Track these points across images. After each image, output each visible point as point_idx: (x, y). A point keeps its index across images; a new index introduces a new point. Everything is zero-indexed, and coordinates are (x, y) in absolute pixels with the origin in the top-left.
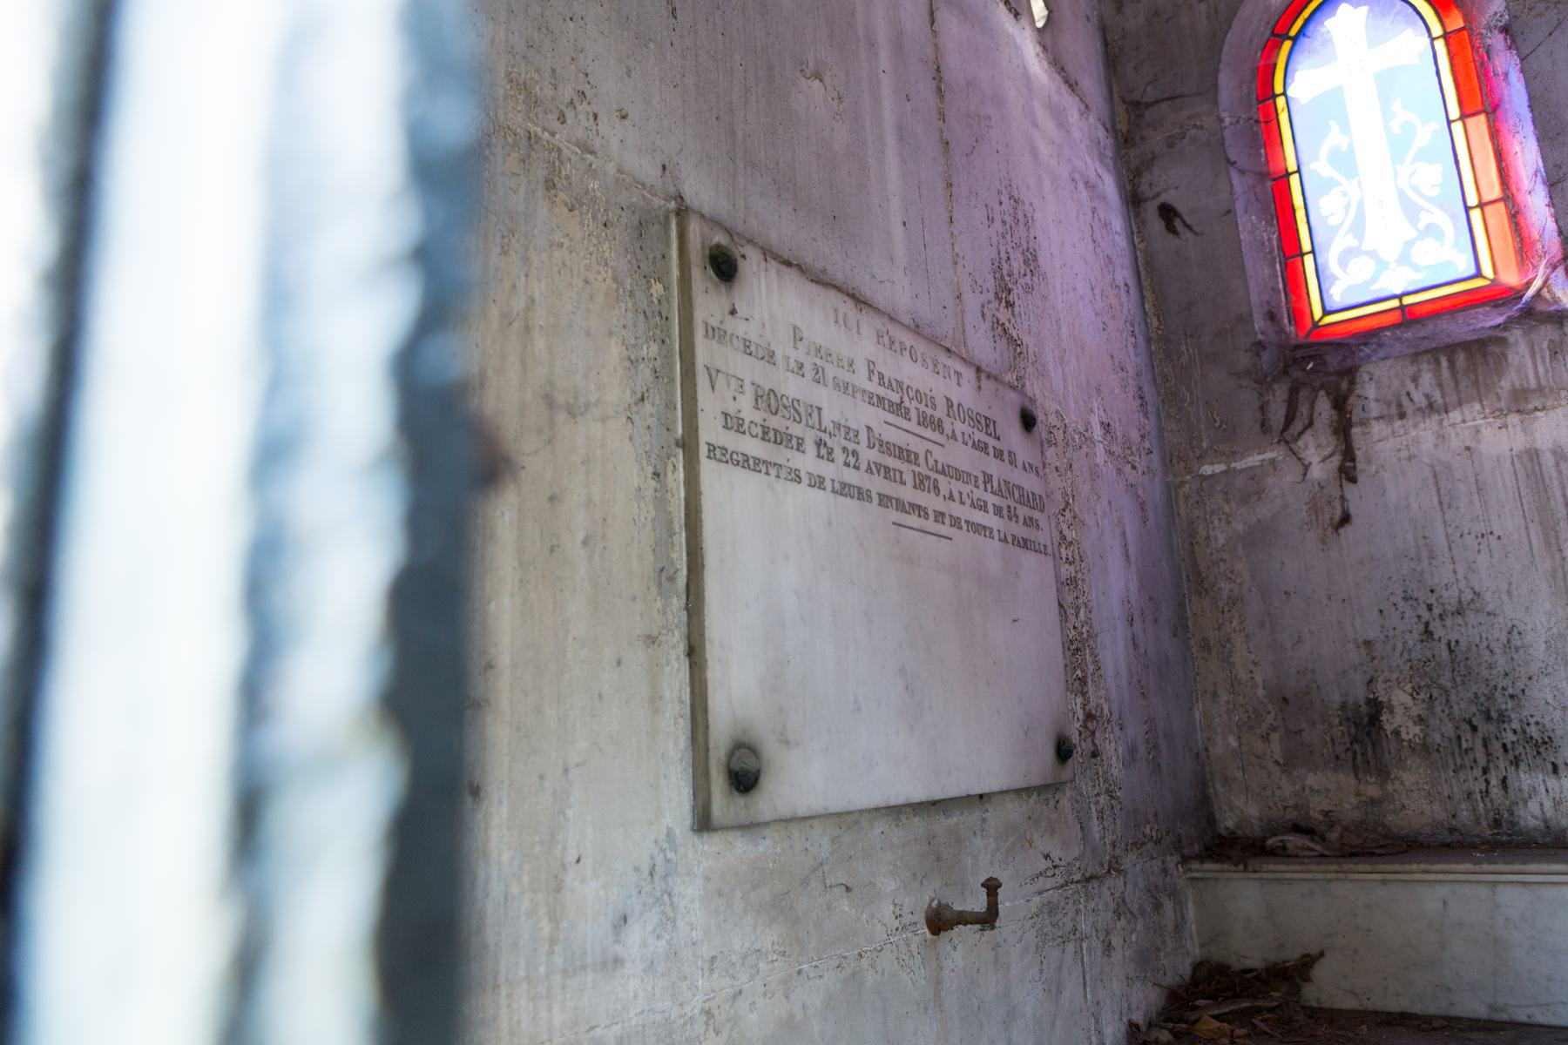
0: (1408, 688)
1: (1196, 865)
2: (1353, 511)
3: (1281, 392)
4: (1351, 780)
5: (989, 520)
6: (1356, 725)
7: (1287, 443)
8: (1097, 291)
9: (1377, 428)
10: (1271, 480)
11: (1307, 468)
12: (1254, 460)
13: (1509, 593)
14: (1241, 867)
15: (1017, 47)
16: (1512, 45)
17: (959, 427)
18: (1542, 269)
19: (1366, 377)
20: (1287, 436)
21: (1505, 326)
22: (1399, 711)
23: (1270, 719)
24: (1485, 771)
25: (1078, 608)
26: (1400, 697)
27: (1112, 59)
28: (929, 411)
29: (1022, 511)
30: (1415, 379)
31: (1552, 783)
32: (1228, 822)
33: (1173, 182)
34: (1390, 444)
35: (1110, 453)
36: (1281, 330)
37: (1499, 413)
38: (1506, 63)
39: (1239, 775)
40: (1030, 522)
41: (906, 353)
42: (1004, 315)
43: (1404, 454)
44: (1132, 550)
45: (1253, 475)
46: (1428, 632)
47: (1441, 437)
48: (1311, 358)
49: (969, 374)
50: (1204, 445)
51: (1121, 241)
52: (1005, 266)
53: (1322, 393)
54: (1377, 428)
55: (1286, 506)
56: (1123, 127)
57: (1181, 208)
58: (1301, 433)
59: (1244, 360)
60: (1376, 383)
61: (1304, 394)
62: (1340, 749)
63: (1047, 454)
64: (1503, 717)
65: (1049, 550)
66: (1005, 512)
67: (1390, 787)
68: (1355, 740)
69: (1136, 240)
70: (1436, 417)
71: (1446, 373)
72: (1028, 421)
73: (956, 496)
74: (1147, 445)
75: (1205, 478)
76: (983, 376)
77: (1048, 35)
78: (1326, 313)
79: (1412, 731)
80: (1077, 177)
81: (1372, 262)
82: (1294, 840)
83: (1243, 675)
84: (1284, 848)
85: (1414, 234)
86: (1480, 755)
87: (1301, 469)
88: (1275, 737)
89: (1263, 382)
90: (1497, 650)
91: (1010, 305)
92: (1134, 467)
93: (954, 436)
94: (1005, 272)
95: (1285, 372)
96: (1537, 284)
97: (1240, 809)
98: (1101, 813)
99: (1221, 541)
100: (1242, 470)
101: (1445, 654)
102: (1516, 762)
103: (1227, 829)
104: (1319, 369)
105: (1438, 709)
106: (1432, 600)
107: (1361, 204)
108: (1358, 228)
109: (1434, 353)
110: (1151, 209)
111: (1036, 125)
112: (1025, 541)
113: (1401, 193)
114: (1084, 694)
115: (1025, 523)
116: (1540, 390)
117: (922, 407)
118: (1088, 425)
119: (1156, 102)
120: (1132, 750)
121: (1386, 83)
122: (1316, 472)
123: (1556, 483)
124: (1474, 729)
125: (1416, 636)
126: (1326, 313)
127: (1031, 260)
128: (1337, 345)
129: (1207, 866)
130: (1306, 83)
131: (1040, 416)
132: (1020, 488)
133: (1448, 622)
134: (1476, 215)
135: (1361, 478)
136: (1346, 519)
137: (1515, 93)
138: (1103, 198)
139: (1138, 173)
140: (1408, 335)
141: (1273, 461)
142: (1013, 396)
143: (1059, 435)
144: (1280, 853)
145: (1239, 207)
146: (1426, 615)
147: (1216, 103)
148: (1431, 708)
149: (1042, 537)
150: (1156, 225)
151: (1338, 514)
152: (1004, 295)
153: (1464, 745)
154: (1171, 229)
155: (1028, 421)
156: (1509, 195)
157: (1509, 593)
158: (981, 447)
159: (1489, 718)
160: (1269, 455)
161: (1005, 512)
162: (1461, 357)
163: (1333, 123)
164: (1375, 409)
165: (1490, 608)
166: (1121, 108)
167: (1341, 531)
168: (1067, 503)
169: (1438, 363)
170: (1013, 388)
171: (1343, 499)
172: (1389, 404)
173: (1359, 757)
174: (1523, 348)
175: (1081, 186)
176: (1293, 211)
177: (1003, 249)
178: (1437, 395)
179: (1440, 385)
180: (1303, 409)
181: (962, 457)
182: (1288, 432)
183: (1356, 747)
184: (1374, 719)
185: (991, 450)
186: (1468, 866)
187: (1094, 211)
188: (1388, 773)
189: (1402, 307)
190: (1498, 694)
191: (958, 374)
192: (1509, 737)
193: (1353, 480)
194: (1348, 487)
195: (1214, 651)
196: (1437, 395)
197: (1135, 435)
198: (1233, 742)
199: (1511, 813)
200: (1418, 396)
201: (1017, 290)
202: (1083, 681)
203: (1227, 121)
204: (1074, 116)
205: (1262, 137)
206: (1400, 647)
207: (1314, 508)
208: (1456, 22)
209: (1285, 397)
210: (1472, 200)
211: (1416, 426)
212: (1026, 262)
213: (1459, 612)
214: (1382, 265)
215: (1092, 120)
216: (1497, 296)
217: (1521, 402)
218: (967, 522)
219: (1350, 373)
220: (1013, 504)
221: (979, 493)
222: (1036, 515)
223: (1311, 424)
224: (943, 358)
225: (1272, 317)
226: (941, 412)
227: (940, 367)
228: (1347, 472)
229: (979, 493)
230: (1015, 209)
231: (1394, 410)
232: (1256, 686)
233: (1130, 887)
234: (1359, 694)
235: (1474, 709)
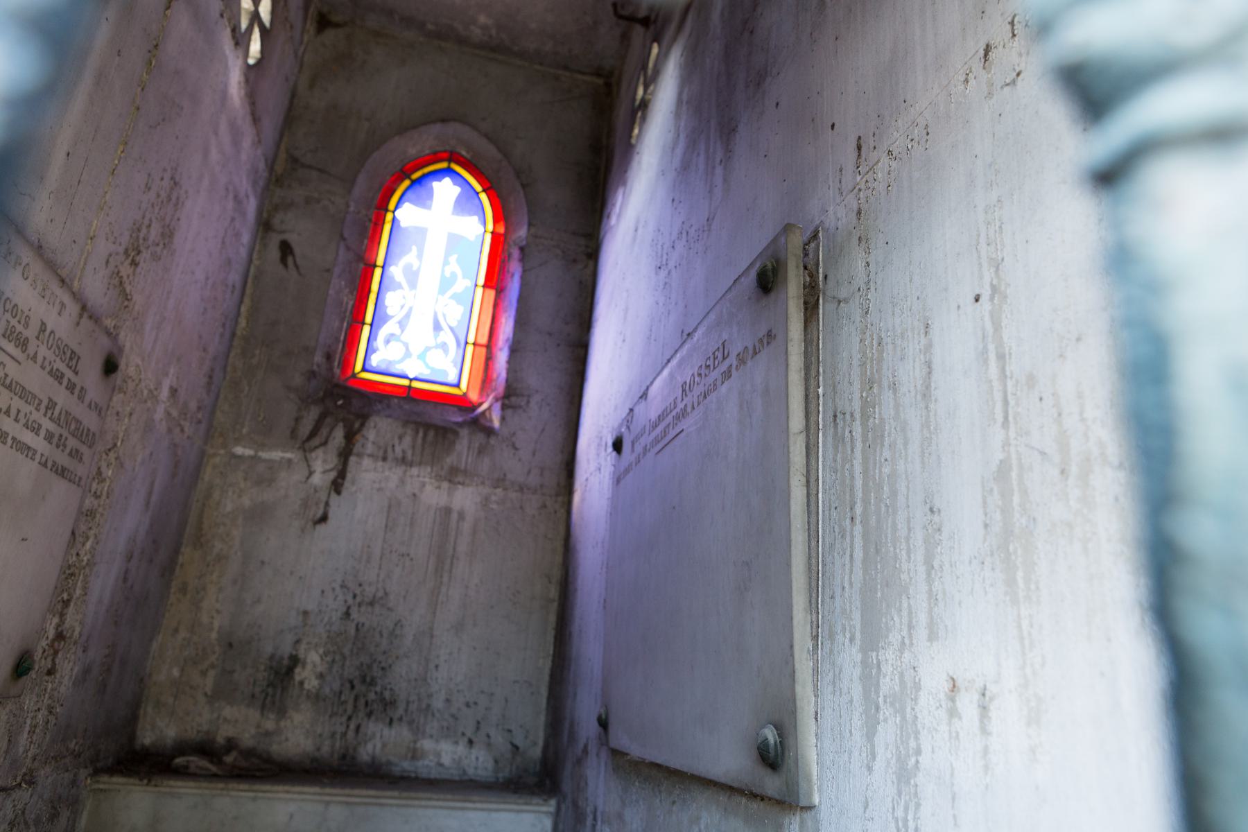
0: (321, 651)
1: (105, 778)
2: (330, 515)
3: (313, 413)
4: (257, 715)
5: (37, 442)
6: (277, 673)
7: (305, 451)
8: (210, 282)
9: (367, 462)
10: (283, 474)
11: (311, 473)
12: (276, 455)
13: (405, 597)
14: (145, 781)
15: (226, 67)
16: (522, 260)
17: (43, 351)
18: (491, 397)
19: (372, 425)
20: (307, 446)
21: (461, 425)
22: (309, 667)
23: (213, 658)
24: (350, 718)
25: (88, 538)
26: (313, 658)
27: (290, 119)
28: (19, 328)
29: (72, 443)
30: (400, 438)
31: (386, 732)
32: (146, 738)
33: (299, 229)
34: (371, 476)
35: (168, 414)
36: (331, 369)
37: (439, 478)
38: (515, 267)
39: (171, 700)
40: (75, 454)
41: (20, 269)
42: (126, 270)
43: (376, 486)
44: (154, 498)
45: (271, 465)
46: (347, 614)
47: (402, 482)
48: (344, 397)
49: (73, 308)
50: (244, 431)
51: (243, 252)
52: (144, 231)
53: (341, 424)
54: (367, 462)
55: (286, 496)
56: (279, 168)
57: (297, 250)
58: (316, 447)
59: (298, 380)
60: (380, 429)
61: (329, 420)
62: (258, 690)
63: (115, 399)
64: (373, 682)
65: (83, 483)
66: (55, 440)
67: (282, 724)
68: (271, 684)
69: (255, 256)
70: (403, 468)
71: (419, 441)
72: (110, 367)
73: (13, 412)
74: (200, 416)
75: (234, 456)
76: (85, 315)
77: (253, 73)
78: (364, 369)
79: (312, 683)
80: (231, 188)
81: (404, 349)
82: (196, 762)
83: (205, 619)
84: (187, 767)
85: (433, 343)
86: (350, 707)
87: (307, 473)
88: (212, 673)
89: (306, 401)
90: (385, 635)
91: (134, 264)
92: (182, 431)
93: (34, 358)
94: (142, 235)
95: (322, 400)
96: (485, 406)
97: (159, 729)
98: (34, 727)
99: (229, 508)
100: (265, 461)
101: (353, 632)
102: (369, 715)
103: (143, 745)
104: (348, 406)
105: (334, 670)
106: (358, 592)
107: (411, 309)
108: (402, 324)
109: (418, 425)
110: (275, 240)
111: (216, 134)
112: (64, 469)
113: (436, 314)
114: (62, 615)
115: (70, 454)
116: (465, 472)
117: (14, 322)
118: (159, 385)
119: (310, 167)
120: (86, 671)
121: (454, 241)
122: (317, 479)
123: (453, 533)
124: (353, 687)
125: (339, 614)
126: (364, 369)
127: (168, 234)
128: (362, 395)
129: (115, 779)
130: (407, 214)
131: (122, 366)
132: (78, 422)
133: (363, 609)
134: (470, 349)
135: (344, 493)
136: (324, 519)
137: (514, 287)
138: (244, 214)
139: (276, 208)
140: (407, 407)
141: (290, 461)
142: (105, 341)
143: (131, 385)
144: (182, 773)
145: (337, 270)
146: (350, 601)
147: (350, 192)
148: (330, 669)
149: (80, 470)
150: (274, 253)
151: (320, 513)
152: (133, 254)
153: (343, 698)
154: (283, 260)
155: (110, 367)
156: (490, 346)
157: (405, 597)
158: (58, 376)
159: (363, 681)
160: (289, 455)
161: (55, 440)
162: (431, 433)
163: (414, 248)
164: (370, 448)
165: (391, 605)
166: (282, 155)
167: (318, 527)
168: (115, 445)
169: (417, 432)
170: (109, 334)
171: (327, 504)
172: (379, 448)
173: (269, 698)
174: (465, 442)
175: (231, 196)
176: (369, 292)
177: (148, 216)
178: (409, 453)
179: (413, 447)
180: (324, 431)
181: (34, 378)
182: (308, 443)
183: (270, 690)
184: (290, 670)
185: (65, 382)
186: (396, 794)
187: (233, 219)
188: (286, 712)
189: (410, 387)
190: (375, 666)
191: (63, 305)
192: (372, 696)
193: (338, 493)
194: (334, 495)
195: (188, 596)
196: (409, 453)
197: (193, 405)
198: (176, 672)
199: (355, 749)
200: (398, 449)
201: (146, 255)
202: (66, 603)
203: (352, 209)
204: (247, 142)
205: (369, 233)
206: (326, 619)
207: (305, 504)
208: (501, 230)
209: (316, 417)
210: (471, 339)
211: (390, 469)
212: (163, 235)
213: (371, 604)
214: (408, 354)
215: (259, 152)
216: (461, 403)
217: (453, 476)
218: (14, 439)
219: (364, 418)
220: (65, 434)
221: (37, 416)
222: (84, 449)
223: (325, 443)
224: (55, 286)
225: (329, 357)
226: (30, 333)
227: (48, 293)
228: (337, 486)
229: (37, 416)
230: (172, 189)
231: (381, 454)
232: (211, 629)
233: (35, 798)
234: (286, 649)
235: (357, 673)
